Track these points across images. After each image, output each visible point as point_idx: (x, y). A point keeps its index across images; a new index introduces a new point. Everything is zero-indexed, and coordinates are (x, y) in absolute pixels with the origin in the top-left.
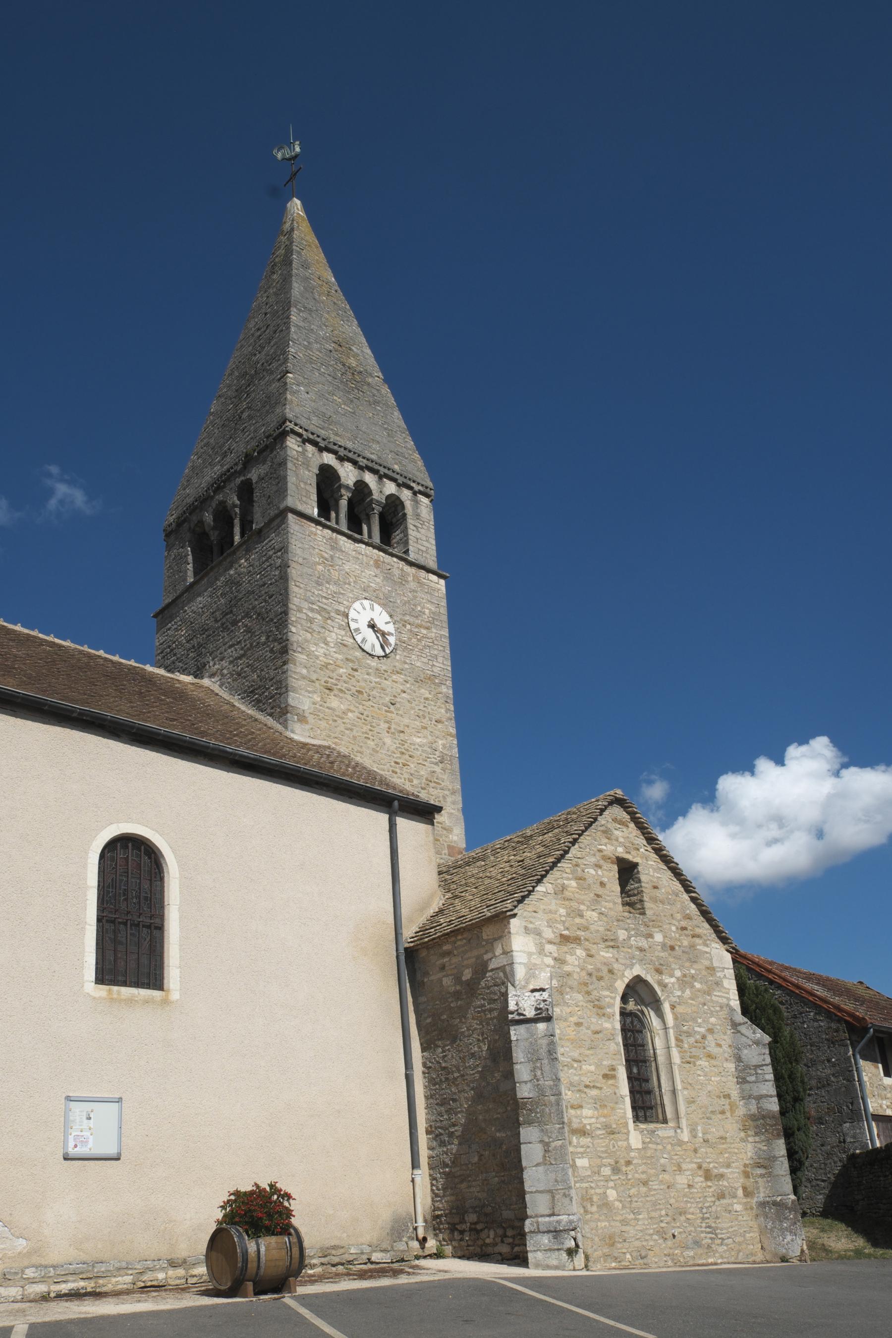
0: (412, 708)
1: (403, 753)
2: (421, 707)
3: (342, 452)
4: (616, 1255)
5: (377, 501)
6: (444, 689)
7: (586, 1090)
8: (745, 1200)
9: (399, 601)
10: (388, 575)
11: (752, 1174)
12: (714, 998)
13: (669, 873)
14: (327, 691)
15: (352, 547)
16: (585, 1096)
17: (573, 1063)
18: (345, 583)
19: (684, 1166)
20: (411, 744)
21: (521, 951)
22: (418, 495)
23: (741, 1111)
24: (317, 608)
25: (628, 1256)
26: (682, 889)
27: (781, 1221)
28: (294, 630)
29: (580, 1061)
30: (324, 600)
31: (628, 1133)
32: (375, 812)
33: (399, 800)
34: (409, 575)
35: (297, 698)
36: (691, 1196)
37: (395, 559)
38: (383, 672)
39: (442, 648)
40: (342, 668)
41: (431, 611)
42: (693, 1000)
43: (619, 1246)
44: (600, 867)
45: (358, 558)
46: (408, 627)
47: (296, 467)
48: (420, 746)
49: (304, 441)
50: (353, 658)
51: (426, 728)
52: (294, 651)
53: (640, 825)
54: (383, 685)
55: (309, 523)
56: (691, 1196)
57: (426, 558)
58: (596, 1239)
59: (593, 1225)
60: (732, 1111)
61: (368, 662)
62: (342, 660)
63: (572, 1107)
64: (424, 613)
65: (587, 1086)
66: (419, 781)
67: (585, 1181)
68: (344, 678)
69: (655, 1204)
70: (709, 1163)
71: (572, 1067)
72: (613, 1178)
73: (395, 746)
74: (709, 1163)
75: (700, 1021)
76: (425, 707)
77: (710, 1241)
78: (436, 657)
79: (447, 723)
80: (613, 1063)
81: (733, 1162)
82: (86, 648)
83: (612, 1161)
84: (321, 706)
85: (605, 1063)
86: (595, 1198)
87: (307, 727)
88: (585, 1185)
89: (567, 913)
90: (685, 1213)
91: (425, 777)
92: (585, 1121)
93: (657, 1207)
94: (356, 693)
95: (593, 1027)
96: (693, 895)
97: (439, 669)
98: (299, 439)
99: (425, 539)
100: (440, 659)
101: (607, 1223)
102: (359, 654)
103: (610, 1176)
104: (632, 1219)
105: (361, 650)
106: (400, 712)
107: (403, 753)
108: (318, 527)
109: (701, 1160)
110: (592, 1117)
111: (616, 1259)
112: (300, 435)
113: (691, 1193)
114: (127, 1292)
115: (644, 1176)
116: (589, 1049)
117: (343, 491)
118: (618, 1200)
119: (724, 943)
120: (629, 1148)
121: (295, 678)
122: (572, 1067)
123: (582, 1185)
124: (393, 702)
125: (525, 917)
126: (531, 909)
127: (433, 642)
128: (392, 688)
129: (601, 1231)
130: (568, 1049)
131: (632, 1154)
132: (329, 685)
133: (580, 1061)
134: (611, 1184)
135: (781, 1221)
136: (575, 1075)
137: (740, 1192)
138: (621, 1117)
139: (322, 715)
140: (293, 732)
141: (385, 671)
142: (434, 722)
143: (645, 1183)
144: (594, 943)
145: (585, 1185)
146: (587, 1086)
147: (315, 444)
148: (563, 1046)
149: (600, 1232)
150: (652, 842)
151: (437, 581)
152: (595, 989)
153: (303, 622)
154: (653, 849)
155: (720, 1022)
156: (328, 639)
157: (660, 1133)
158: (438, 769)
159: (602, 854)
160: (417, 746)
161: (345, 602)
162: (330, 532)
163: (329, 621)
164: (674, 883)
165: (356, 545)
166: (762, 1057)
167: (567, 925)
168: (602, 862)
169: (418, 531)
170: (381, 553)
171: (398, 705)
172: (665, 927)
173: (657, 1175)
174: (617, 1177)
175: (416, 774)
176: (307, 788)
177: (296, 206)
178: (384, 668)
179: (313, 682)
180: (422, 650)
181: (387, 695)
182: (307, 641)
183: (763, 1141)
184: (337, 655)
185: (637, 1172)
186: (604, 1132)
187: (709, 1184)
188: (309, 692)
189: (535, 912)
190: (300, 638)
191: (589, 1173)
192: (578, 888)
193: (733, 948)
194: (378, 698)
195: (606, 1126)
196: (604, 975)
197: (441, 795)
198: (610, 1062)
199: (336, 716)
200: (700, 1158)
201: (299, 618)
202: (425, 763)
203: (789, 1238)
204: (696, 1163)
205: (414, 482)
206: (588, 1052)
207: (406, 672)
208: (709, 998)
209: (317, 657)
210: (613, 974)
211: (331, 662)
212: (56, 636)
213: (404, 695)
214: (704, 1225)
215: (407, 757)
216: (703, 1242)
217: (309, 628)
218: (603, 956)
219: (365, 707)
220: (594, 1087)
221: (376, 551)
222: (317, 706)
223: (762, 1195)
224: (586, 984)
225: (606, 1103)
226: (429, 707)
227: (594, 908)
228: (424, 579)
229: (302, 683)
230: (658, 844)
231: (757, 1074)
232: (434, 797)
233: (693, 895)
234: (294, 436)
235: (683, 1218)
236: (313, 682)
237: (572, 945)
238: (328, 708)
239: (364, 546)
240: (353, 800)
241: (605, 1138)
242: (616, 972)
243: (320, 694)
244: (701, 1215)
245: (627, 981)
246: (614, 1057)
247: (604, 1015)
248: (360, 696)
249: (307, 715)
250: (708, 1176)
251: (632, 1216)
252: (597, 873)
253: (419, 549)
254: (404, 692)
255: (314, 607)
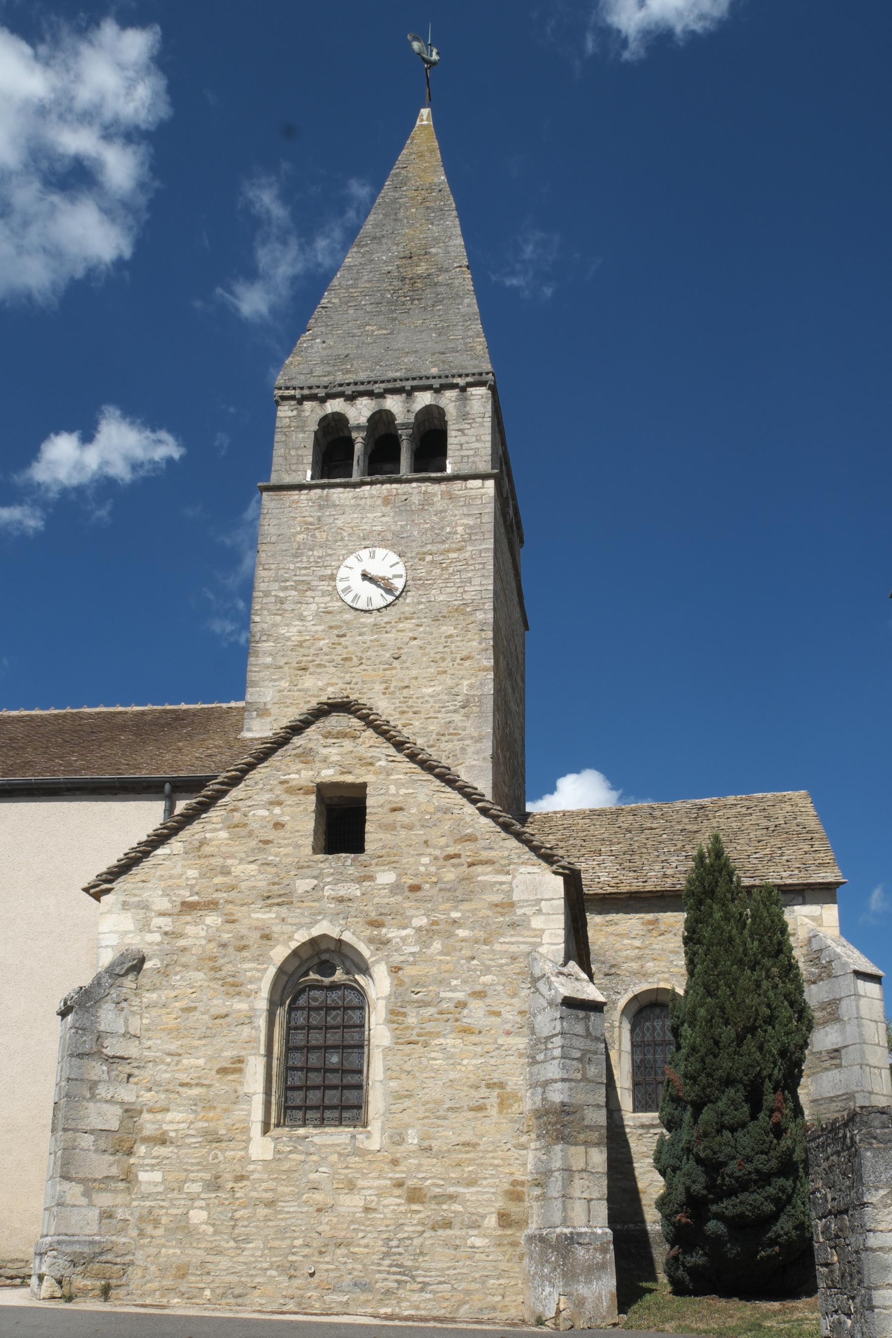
0: (424, 655)
1: (403, 712)
2: (441, 649)
3: (349, 391)
4: (183, 1289)
5: (403, 425)
6: (480, 616)
7: (181, 1089)
8: (499, 1232)
9: (416, 533)
10: (403, 507)
11: (529, 1195)
12: (497, 947)
13: (438, 782)
14: (301, 672)
15: (351, 494)
16: (177, 1096)
17: (165, 1056)
18: (336, 541)
19: (361, 1183)
20: (417, 698)
21: (110, 932)
22: (468, 389)
23: (529, 1102)
24: (292, 583)
25: (207, 1293)
26: (464, 801)
27: (543, 1266)
28: (257, 619)
29: (180, 1055)
30: (303, 572)
31: (248, 1140)
32: (149, 803)
33: (169, 782)
34: (435, 495)
35: (257, 691)
36: (368, 1223)
37: (414, 485)
38: (384, 625)
39: (481, 566)
40: (323, 639)
41: (466, 526)
42: (447, 954)
43: (193, 1278)
44: (279, 803)
45: (359, 505)
46: (429, 558)
47: (286, 436)
48: (433, 696)
49: (301, 401)
50: (339, 624)
51: (445, 672)
52: (257, 642)
53: (379, 730)
54: (382, 641)
55: (290, 493)
56: (368, 1223)
57: (474, 462)
58: (153, 1268)
59: (152, 1251)
60: (503, 1104)
61: (362, 620)
62: (323, 631)
63: (150, 1111)
64: (456, 533)
65: (182, 1085)
66: (426, 739)
67: (150, 1199)
68: (325, 649)
69: (281, 1232)
70: (425, 1179)
71: (163, 1062)
72: (203, 1196)
73: (393, 707)
74: (425, 1179)
75: (454, 982)
76: (445, 647)
77: (395, 1285)
78: (470, 581)
79: (478, 657)
80: (242, 1054)
81: (486, 1178)
82: (69, 710)
83: (207, 1176)
84: (290, 691)
85: (225, 1054)
86: (164, 1220)
87: (269, 719)
88: (148, 1204)
89: (200, 874)
90: (348, 1245)
91: (435, 732)
92: (165, 1127)
93: (287, 1235)
94: (342, 662)
95: (214, 1011)
96: (479, 805)
97: (473, 593)
98: (293, 403)
99: (474, 439)
100: (477, 581)
101: (178, 1251)
102: (348, 616)
103: (199, 1194)
104: (231, 1248)
105: (352, 611)
106: (407, 665)
107: (403, 712)
108: (303, 492)
109: (404, 1175)
110: (183, 1122)
111: (183, 1294)
112: (292, 398)
113: (369, 1219)
114: (268, 1312)
115: (269, 1195)
116: (200, 1039)
117: (354, 435)
118: (206, 1223)
119: (551, 863)
120: (246, 1160)
121: (255, 672)
122: (163, 1062)
123: (143, 1204)
124: (396, 656)
125: (125, 891)
126: (138, 878)
127: (467, 564)
128: (396, 639)
129: (164, 1259)
130: (159, 1042)
131: (251, 1167)
132: (303, 664)
133: (180, 1055)
134: (198, 1203)
135: (543, 1266)
136: (166, 1071)
137: (492, 1221)
138: (241, 1121)
139: (289, 701)
140: (249, 730)
141: (386, 623)
142: (458, 661)
143: (270, 1204)
144: (242, 905)
145: (148, 1204)
146: (182, 1085)
147: (313, 398)
148: (149, 1039)
149: (161, 1260)
150: (401, 747)
151: (480, 485)
152: (230, 962)
153: (271, 607)
154: (408, 756)
155: (503, 980)
156: (305, 613)
157: (316, 1140)
158: (457, 717)
159: (285, 786)
160: (427, 698)
161: (333, 563)
162: (318, 491)
163: (308, 593)
164: (448, 795)
165: (357, 490)
166: (553, 1024)
167: (196, 889)
168: (284, 797)
169: (464, 435)
170: (394, 486)
171: (404, 658)
172: (404, 861)
173: (300, 1194)
174: (214, 1195)
175: (423, 731)
176: (55, 798)
177: (425, 112)
178: (386, 619)
179: (280, 667)
180: (448, 579)
181: (386, 651)
182: (275, 625)
183: (543, 1148)
184: (317, 628)
185: (255, 1189)
186: (200, 1140)
187: (415, 1207)
188: (275, 680)
189: (144, 881)
190: (266, 625)
191: (160, 1189)
192: (229, 839)
193: (563, 867)
194: (373, 658)
195: (205, 1133)
196: (251, 943)
197: (458, 748)
198: (235, 1052)
199: (310, 696)
200: (403, 1172)
201: (266, 603)
202: (439, 715)
203: (548, 1289)
204: (391, 1179)
205: (453, 376)
206: (200, 1042)
207: (419, 615)
208: (487, 948)
209: (288, 639)
210: (269, 939)
211: (308, 638)
212: (153, 704)
213: (415, 642)
214: (387, 1262)
215: (410, 715)
216: (378, 1285)
217: (278, 610)
218: (257, 919)
219: (353, 675)
220: (197, 1085)
221: (388, 486)
222: (285, 693)
223: (534, 1226)
224: (213, 959)
225: (215, 1104)
226: (453, 645)
227: (252, 859)
228: (459, 490)
229: (265, 674)
230: (408, 748)
231: (546, 1049)
232: (447, 753)
233: (479, 805)
234: (286, 403)
235: (342, 1251)
236: (280, 667)
237: (201, 913)
238: (299, 690)
239: (368, 487)
240: (119, 796)
241: (204, 1147)
242: (276, 936)
243: (289, 679)
244: (384, 1249)
245: (294, 945)
246: (246, 1045)
247: (239, 994)
248: (348, 664)
249: (268, 707)
250: (415, 1196)
251: (232, 1244)
252: (271, 813)
253: (463, 457)
254: (415, 639)
255: (288, 584)
